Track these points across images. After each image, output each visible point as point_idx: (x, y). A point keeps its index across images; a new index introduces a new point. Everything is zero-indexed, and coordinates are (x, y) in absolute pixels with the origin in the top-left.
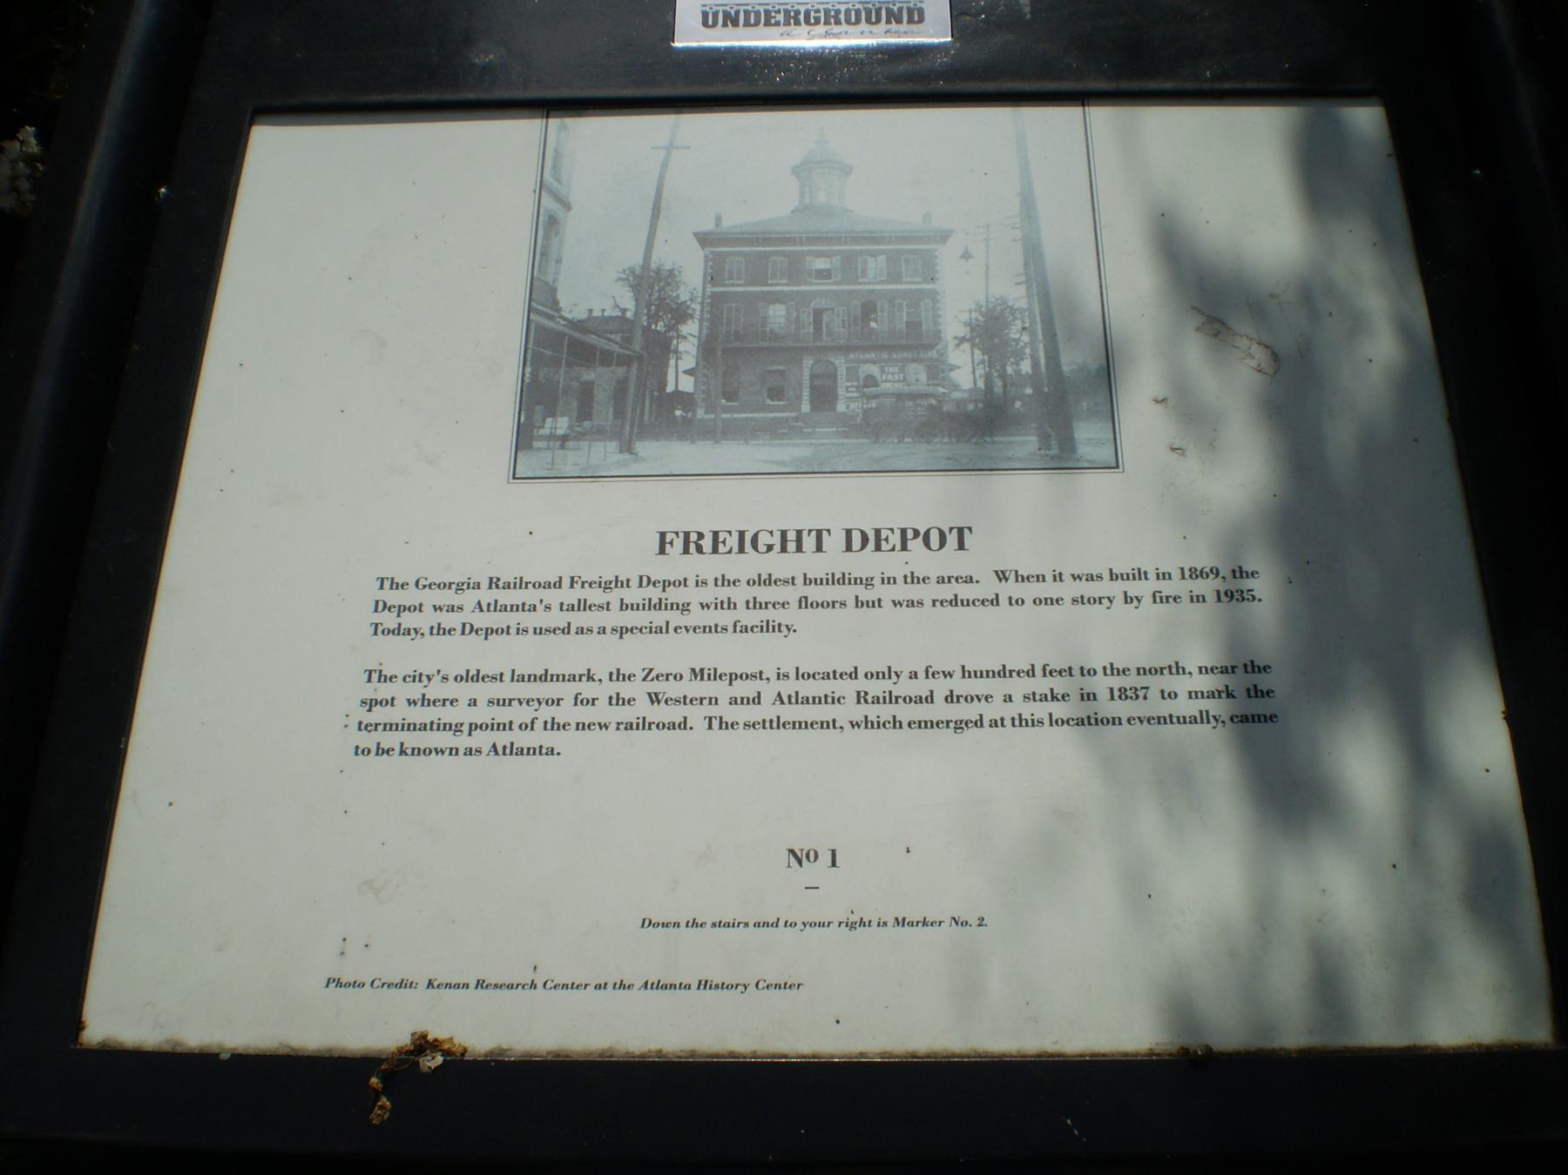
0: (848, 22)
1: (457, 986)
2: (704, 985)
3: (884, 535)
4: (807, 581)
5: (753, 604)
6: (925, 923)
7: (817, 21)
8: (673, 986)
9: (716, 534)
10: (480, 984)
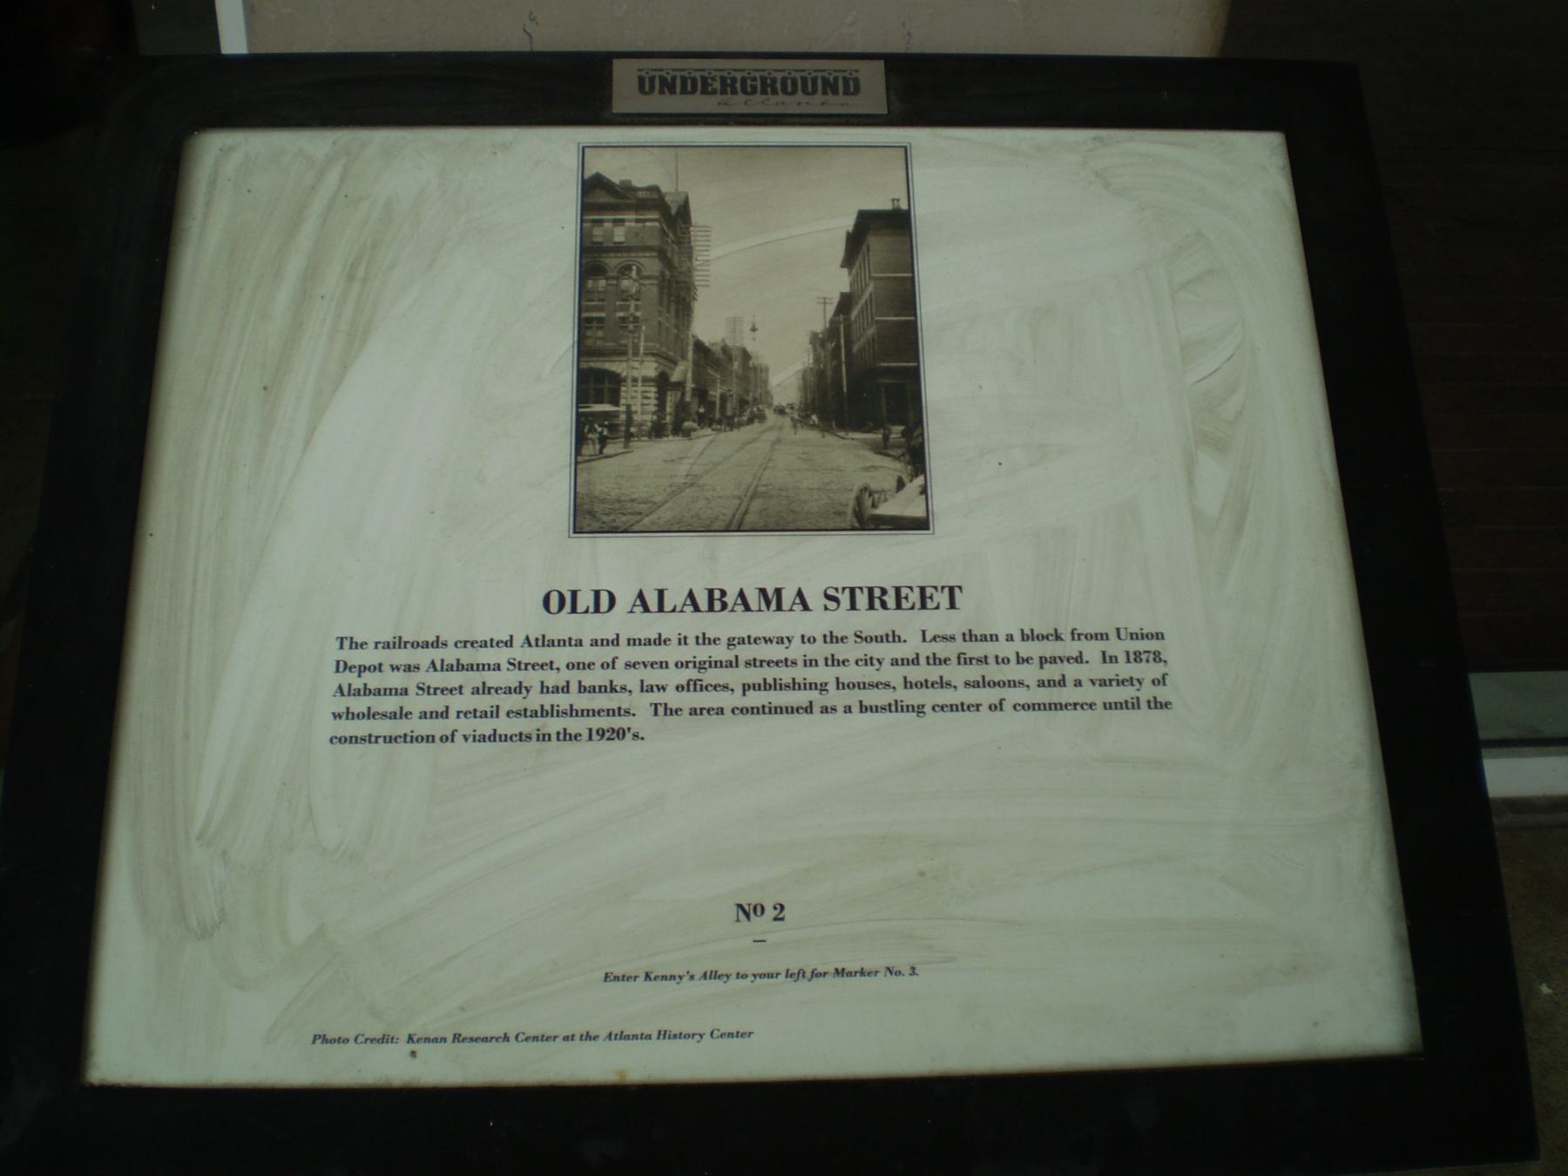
0: (785, 91)
1: (436, 1040)
3: (904, 592)
5: (963, 660)
7: (754, 92)
8: (635, 1037)
9: (898, 590)
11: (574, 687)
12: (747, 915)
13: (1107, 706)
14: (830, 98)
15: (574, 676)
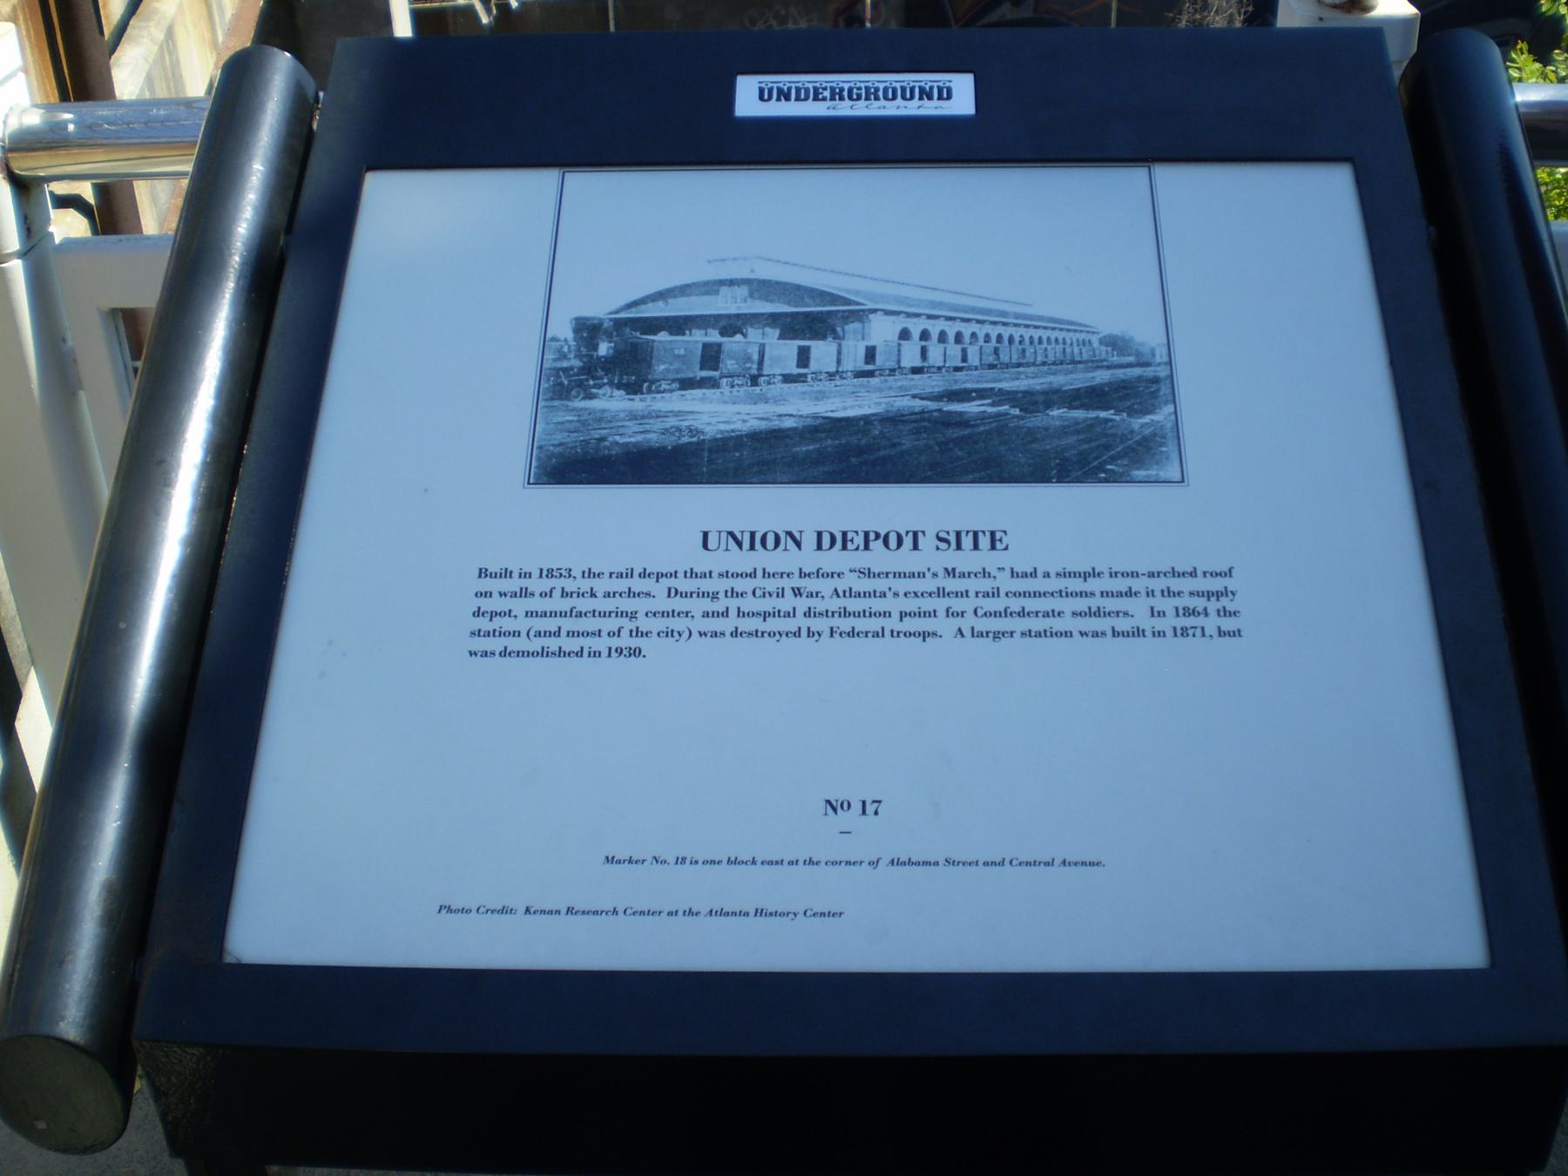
0: (886, 98)
1: (551, 912)
2: (759, 912)
3: (849, 536)
4: (802, 574)
6: (630, 861)
7: (859, 98)
10: (570, 910)
11: (733, 612)
12: (835, 810)
13: (1027, 634)
14: (926, 102)
15: (733, 604)
